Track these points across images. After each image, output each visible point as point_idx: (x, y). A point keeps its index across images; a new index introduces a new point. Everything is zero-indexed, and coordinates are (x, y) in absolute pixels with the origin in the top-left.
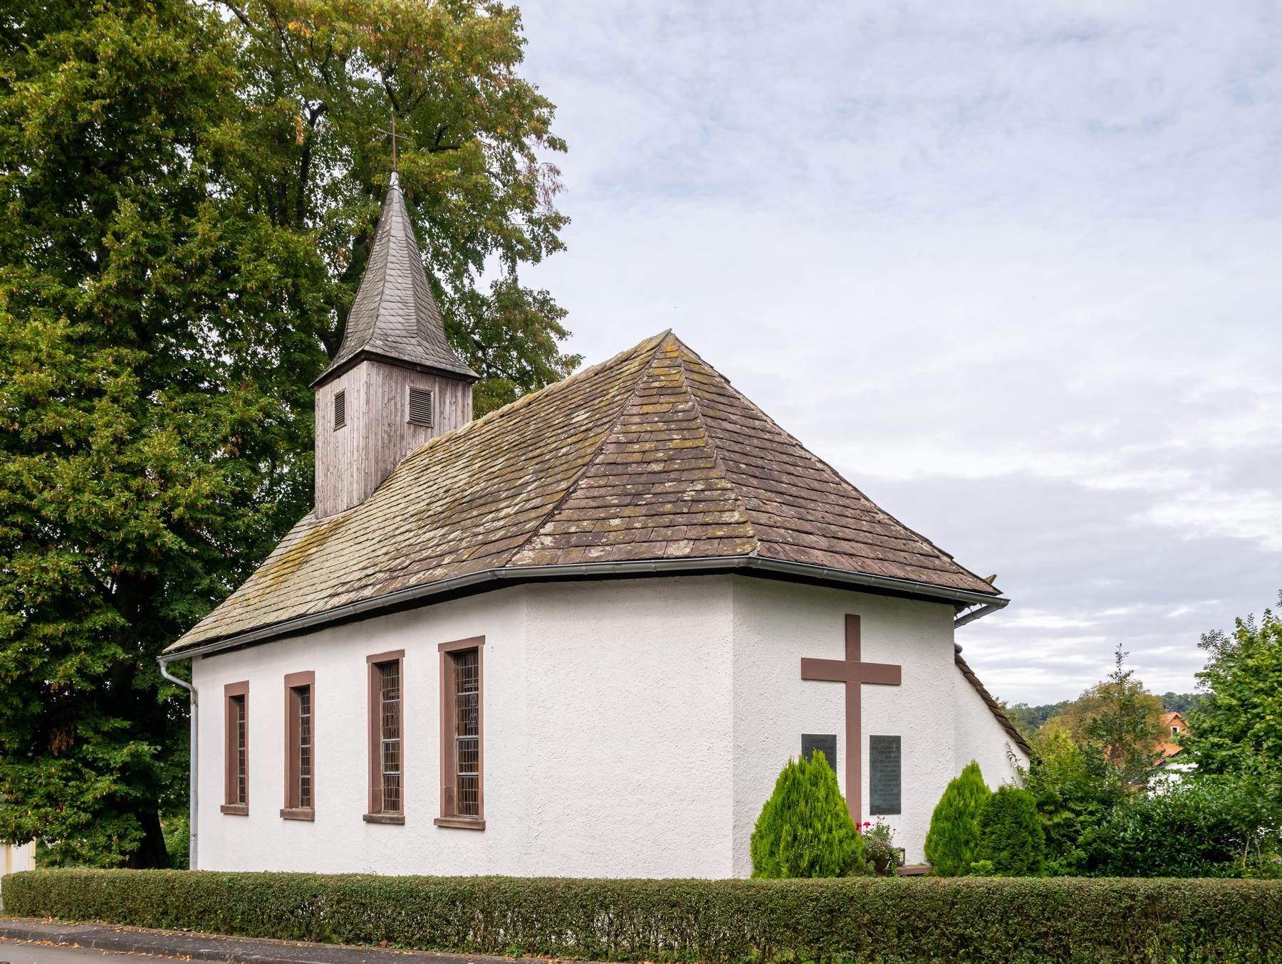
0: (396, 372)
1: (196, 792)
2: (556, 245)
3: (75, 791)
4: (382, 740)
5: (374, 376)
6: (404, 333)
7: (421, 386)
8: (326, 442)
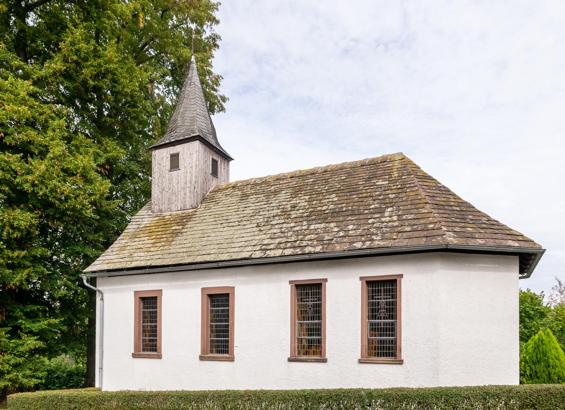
0: (208, 149)
1: (102, 345)
2: (222, 109)
4: (297, 321)
6: (207, 132)
7: (216, 158)
8: (161, 176)
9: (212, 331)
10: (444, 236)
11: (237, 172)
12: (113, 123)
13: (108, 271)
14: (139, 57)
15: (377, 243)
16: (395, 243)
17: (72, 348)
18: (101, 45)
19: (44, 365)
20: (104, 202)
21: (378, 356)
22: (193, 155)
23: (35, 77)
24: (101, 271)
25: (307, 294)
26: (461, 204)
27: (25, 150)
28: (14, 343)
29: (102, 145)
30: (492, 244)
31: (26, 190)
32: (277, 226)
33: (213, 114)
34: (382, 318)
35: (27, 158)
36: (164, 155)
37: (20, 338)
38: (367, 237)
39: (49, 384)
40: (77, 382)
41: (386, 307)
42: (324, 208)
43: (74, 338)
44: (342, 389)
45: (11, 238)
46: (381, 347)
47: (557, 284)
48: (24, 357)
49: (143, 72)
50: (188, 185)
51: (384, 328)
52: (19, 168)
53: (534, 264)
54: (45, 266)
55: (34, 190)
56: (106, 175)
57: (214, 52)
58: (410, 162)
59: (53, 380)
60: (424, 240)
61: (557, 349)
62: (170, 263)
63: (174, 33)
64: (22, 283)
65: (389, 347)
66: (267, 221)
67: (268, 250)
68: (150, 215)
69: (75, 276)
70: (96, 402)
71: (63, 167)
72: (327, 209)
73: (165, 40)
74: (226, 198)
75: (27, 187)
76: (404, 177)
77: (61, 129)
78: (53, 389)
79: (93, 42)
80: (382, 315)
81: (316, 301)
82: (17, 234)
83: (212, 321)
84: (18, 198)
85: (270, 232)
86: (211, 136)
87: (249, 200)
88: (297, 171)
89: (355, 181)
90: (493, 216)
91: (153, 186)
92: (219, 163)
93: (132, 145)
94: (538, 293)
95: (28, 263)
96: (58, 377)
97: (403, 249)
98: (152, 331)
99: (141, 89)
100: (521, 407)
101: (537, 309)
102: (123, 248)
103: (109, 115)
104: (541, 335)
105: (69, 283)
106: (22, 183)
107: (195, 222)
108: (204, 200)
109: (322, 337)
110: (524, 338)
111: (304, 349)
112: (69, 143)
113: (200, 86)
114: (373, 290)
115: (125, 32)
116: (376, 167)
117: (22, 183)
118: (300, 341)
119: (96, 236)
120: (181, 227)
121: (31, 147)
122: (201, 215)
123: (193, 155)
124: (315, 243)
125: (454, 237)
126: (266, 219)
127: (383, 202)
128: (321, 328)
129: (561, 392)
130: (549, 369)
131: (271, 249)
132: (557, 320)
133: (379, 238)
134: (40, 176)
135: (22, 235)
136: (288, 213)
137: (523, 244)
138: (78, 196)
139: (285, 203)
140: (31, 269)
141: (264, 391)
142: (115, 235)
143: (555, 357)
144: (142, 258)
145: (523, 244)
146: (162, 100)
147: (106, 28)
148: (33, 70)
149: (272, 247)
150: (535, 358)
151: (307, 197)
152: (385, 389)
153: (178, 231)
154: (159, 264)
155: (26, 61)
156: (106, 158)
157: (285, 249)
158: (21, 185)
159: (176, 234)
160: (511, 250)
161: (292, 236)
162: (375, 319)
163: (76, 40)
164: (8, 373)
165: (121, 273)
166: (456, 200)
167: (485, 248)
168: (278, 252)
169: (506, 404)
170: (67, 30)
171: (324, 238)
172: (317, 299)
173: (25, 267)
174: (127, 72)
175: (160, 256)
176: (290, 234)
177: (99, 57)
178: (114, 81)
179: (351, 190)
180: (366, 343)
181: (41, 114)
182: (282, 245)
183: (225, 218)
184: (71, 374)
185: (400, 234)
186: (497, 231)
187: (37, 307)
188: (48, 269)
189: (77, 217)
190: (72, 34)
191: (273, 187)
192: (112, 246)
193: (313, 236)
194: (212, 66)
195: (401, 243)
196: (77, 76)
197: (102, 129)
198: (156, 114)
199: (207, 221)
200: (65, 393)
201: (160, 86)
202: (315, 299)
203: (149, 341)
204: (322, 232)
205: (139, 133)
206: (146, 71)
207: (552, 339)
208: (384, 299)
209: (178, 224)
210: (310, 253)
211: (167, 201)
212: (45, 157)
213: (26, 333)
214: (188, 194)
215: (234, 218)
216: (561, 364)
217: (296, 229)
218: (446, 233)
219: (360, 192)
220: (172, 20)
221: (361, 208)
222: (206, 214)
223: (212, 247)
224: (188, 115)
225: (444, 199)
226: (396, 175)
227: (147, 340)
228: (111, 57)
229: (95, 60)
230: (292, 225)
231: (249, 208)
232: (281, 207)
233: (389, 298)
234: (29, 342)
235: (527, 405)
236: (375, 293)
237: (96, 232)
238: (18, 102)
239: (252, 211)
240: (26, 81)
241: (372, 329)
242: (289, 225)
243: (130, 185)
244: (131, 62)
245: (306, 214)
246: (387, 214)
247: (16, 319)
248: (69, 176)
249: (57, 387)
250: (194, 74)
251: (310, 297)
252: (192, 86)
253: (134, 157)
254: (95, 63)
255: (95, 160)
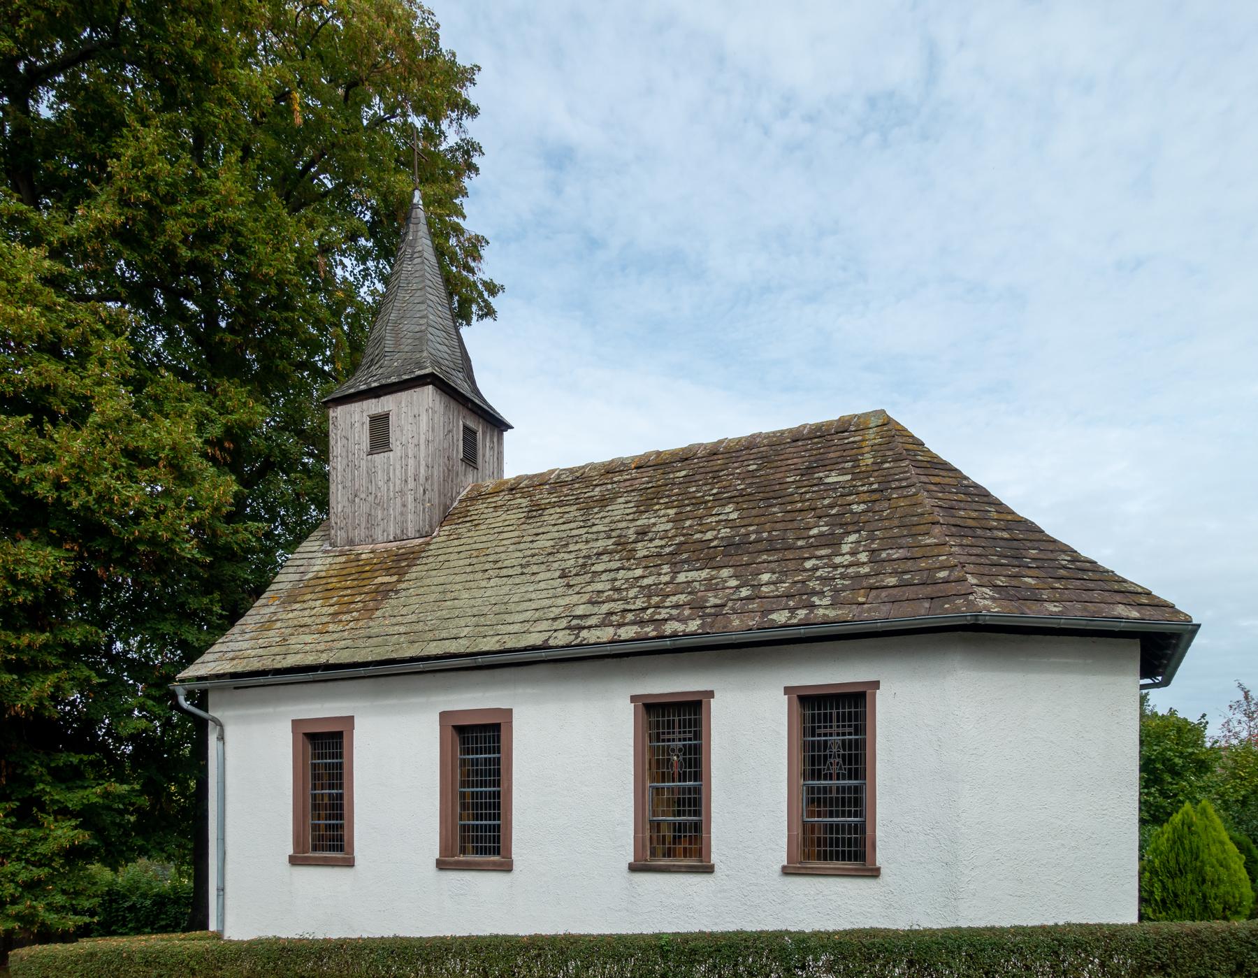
0: (453, 404)
2: (489, 312)
3: (25, 841)
4: (648, 784)
5: (437, 402)
6: (451, 365)
7: (471, 424)
8: (351, 466)
9: (464, 806)
10: (971, 597)
11: (522, 456)
12: (240, 346)
13: (234, 675)
14: (296, 192)
15: (821, 612)
16: (861, 613)
17: (159, 843)
18: (203, 166)
19: (94, 884)
20: (222, 527)
21: (825, 859)
22: (418, 416)
23: (54, 239)
24: (218, 676)
25: (670, 725)
26: (1013, 525)
27: (37, 407)
28: (24, 835)
29: (216, 395)
30: (1079, 614)
31: (40, 496)
32: (604, 577)
33: (469, 324)
34: (835, 776)
35: (41, 424)
36: (357, 417)
37: (40, 826)
38: (801, 599)
39: (114, 923)
40: (176, 918)
41: (842, 752)
42: (709, 535)
43: (164, 824)
44: (742, 932)
45: (11, 604)
46: (831, 839)
47: (1240, 696)
48: (49, 865)
49: (304, 228)
50: (411, 484)
51: (837, 799)
52: (24, 448)
53: (1177, 656)
54: (92, 666)
55: (59, 498)
56: (225, 464)
57: (466, 182)
58: (903, 432)
59: (117, 915)
60: (927, 605)
61: (1222, 843)
62: (370, 659)
63: (379, 140)
64: (41, 704)
65: (850, 839)
66: (584, 565)
67: (584, 628)
68: (326, 552)
69: (160, 685)
70: (204, 964)
71: (126, 447)
72: (716, 538)
73: (353, 153)
74: (495, 514)
75: (43, 490)
76: (887, 465)
77: (118, 359)
78: (122, 934)
79: (186, 158)
80: (834, 770)
81: (690, 739)
82: (24, 596)
83: (463, 784)
84: (27, 515)
85: (589, 588)
86: (460, 375)
87: (546, 518)
88: (650, 454)
89: (778, 476)
90: (1086, 551)
91: (333, 488)
92: (479, 435)
93: (286, 394)
94: (1194, 719)
95: (53, 660)
96: (132, 908)
97: (879, 626)
98: (332, 807)
99: (301, 268)
100: (1137, 972)
101: (1192, 754)
102: (266, 626)
103: (230, 328)
104: (1187, 814)
105: (150, 702)
106: (31, 482)
107: (426, 568)
108: (446, 517)
109: (703, 818)
110: (1151, 816)
111: (664, 843)
112: (137, 390)
113: (433, 260)
114: (813, 715)
115: (260, 135)
116: (824, 444)
117: (31, 482)
118: (656, 826)
119: (206, 600)
120: (395, 578)
121: (51, 399)
122: (440, 552)
123: (418, 416)
124: (687, 612)
125: (993, 598)
126: (581, 561)
127: (838, 520)
128: (700, 799)
129: (1224, 939)
130: (1204, 887)
131: (590, 627)
132: (1234, 776)
133: (826, 601)
134: (73, 465)
135: (36, 597)
136: (629, 547)
137: (1149, 613)
138: (163, 512)
139: (624, 524)
140: (63, 674)
141: (573, 936)
142: (250, 596)
143: (1217, 860)
144: (307, 648)
145: (1149, 613)
146: (351, 290)
147: (216, 126)
148: (48, 222)
149: (593, 621)
150: (1173, 863)
151: (672, 512)
152: (836, 933)
153: (389, 587)
154: (347, 661)
155: (34, 202)
156: (225, 425)
157: (620, 625)
158: (30, 486)
159: (385, 592)
160: (1122, 626)
161: (636, 597)
162: (819, 779)
163: (146, 154)
164: (14, 901)
165: (262, 680)
166: (1002, 516)
167: (1063, 624)
168: (607, 634)
169: (1102, 965)
170: (125, 130)
171: (707, 601)
172: (692, 735)
173: (48, 669)
174: (267, 227)
175: (349, 643)
176: (632, 593)
177: (202, 193)
178: (239, 249)
179: (769, 493)
180: (798, 831)
181: (71, 325)
182: (614, 618)
183: (491, 558)
184: (161, 901)
185: (874, 593)
186: (1091, 585)
187: (79, 757)
188: (101, 673)
189: (162, 559)
190: (137, 139)
191: (598, 489)
192: (242, 621)
193: (682, 598)
194: (464, 217)
195: (875, 612)
196: (152, 238)
197: (216, 361)
198: (339, 325)
199: (452, 564)
200: (136, 944)
201: (346, 261)
202: (688, 735)
203: (324, 828)
204: (702, 588)
205: (302, 366)
206: (310, 225)
207: (1212, 821)
208: (838, 735)
209: (388, 571)
210: (674, 635)
211: (364, 520)
212: (84, 422)
213: (56, 813)
214: (411, 506)
215: (513, 559)
216: (1229, 875)
217: (646, 582)
218: (976, 589)
219: (788, 499)
220: (370, 107)
221: (790, 535)
222: (450, 550)
223: (462, 622)
224: (408, 327)
225: (974, 514)
226: (870, 461)
227: (322, 827)
228: (230, 194)
229: (192, 201)
230: (639, 572)
231: (544, 537)
232: (614, 534)
233: (850, 734)
234: (59, 832)
235: (1149, 968)
236: (819, 722)
237: (207, 592)
238: (17, 297)
239: (552, 543)
240: (34, 250)
241: (811, 801)
242: (630, 574)
243: (282, 484)
244: (276, 206)
245: (668, 550)
246: (845, 548)
247: (31, 783)
248: (139, 467)
249: (131, 929)
250: (420, 234)
251: (677, 730)
252: (416, 261)
253: (292, 423)
254: (192, 208)
255: (200, 428)
